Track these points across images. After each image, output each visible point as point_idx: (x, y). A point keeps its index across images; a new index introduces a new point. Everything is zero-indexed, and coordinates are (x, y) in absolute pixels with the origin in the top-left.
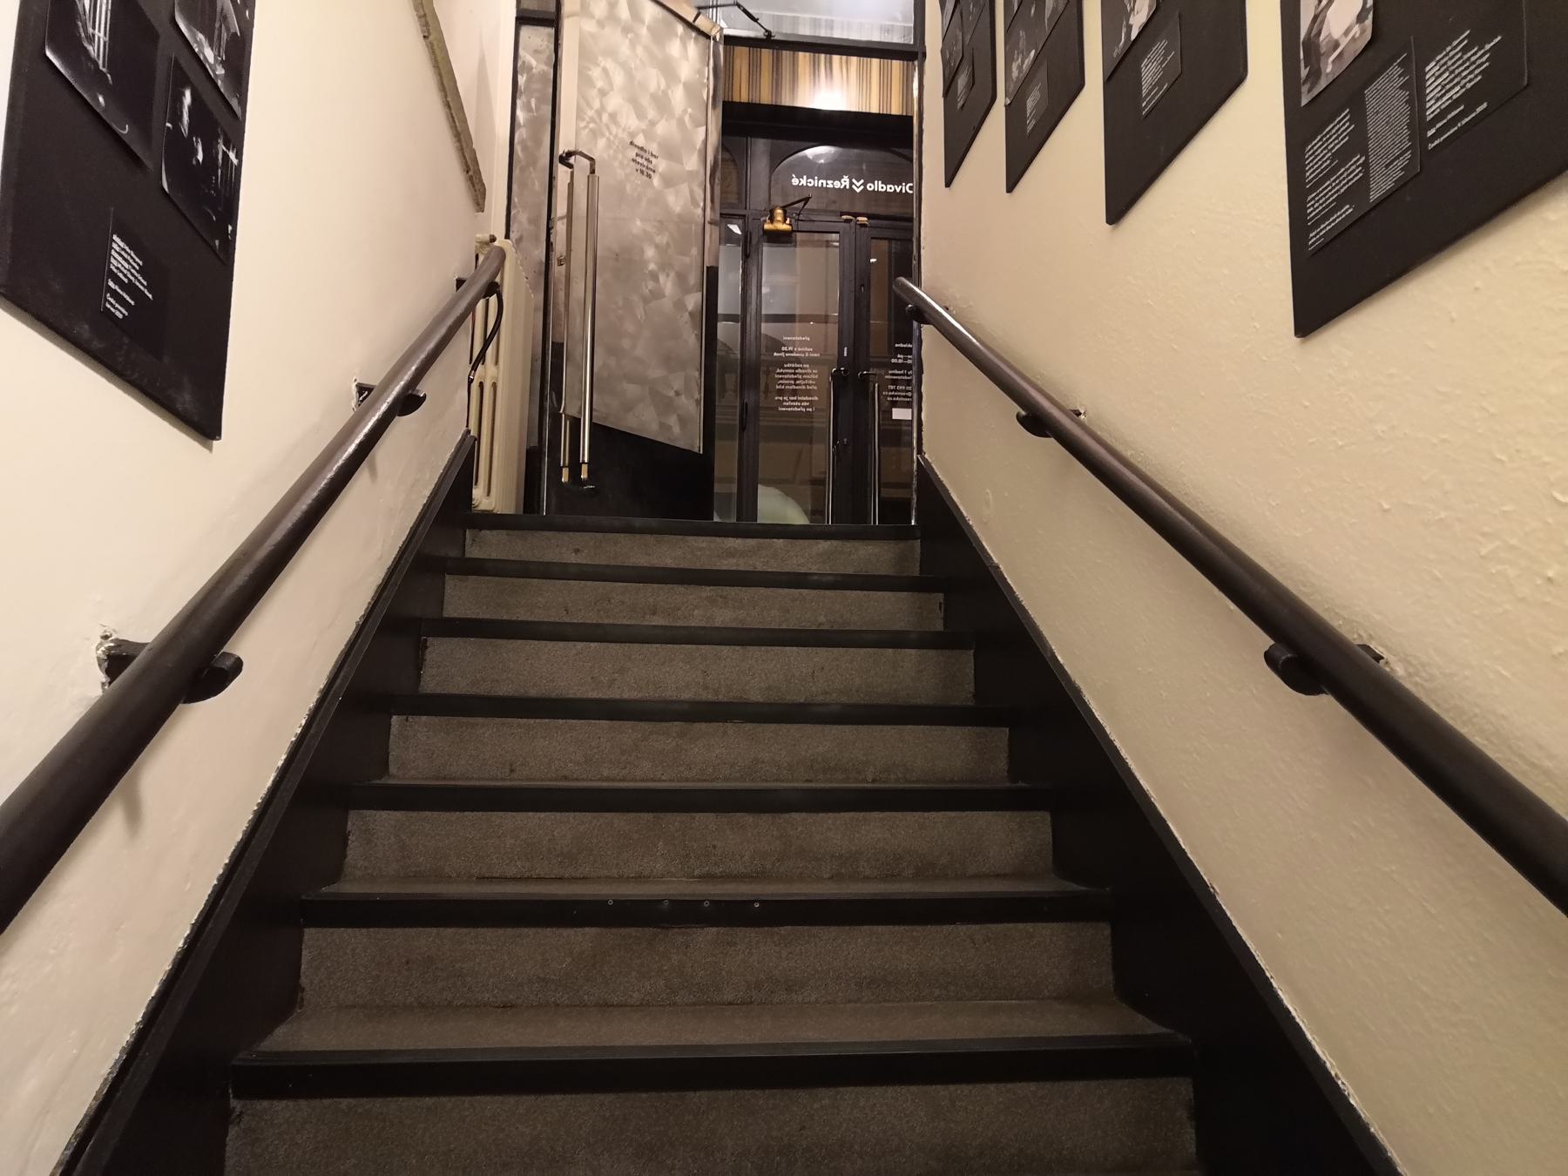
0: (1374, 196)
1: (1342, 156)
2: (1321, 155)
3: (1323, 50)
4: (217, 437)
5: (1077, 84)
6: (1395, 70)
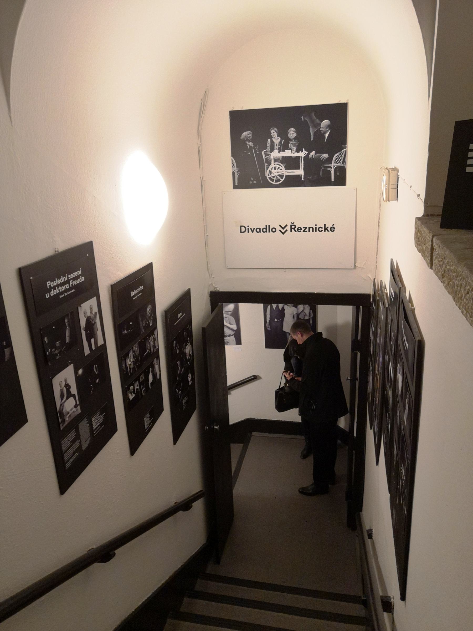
0: (84, 449)
1: (74, 441)
2: (67, 442)
3: (65, 414)
4: (301, 176)
5: (161, 410)
6: (85, 419)
